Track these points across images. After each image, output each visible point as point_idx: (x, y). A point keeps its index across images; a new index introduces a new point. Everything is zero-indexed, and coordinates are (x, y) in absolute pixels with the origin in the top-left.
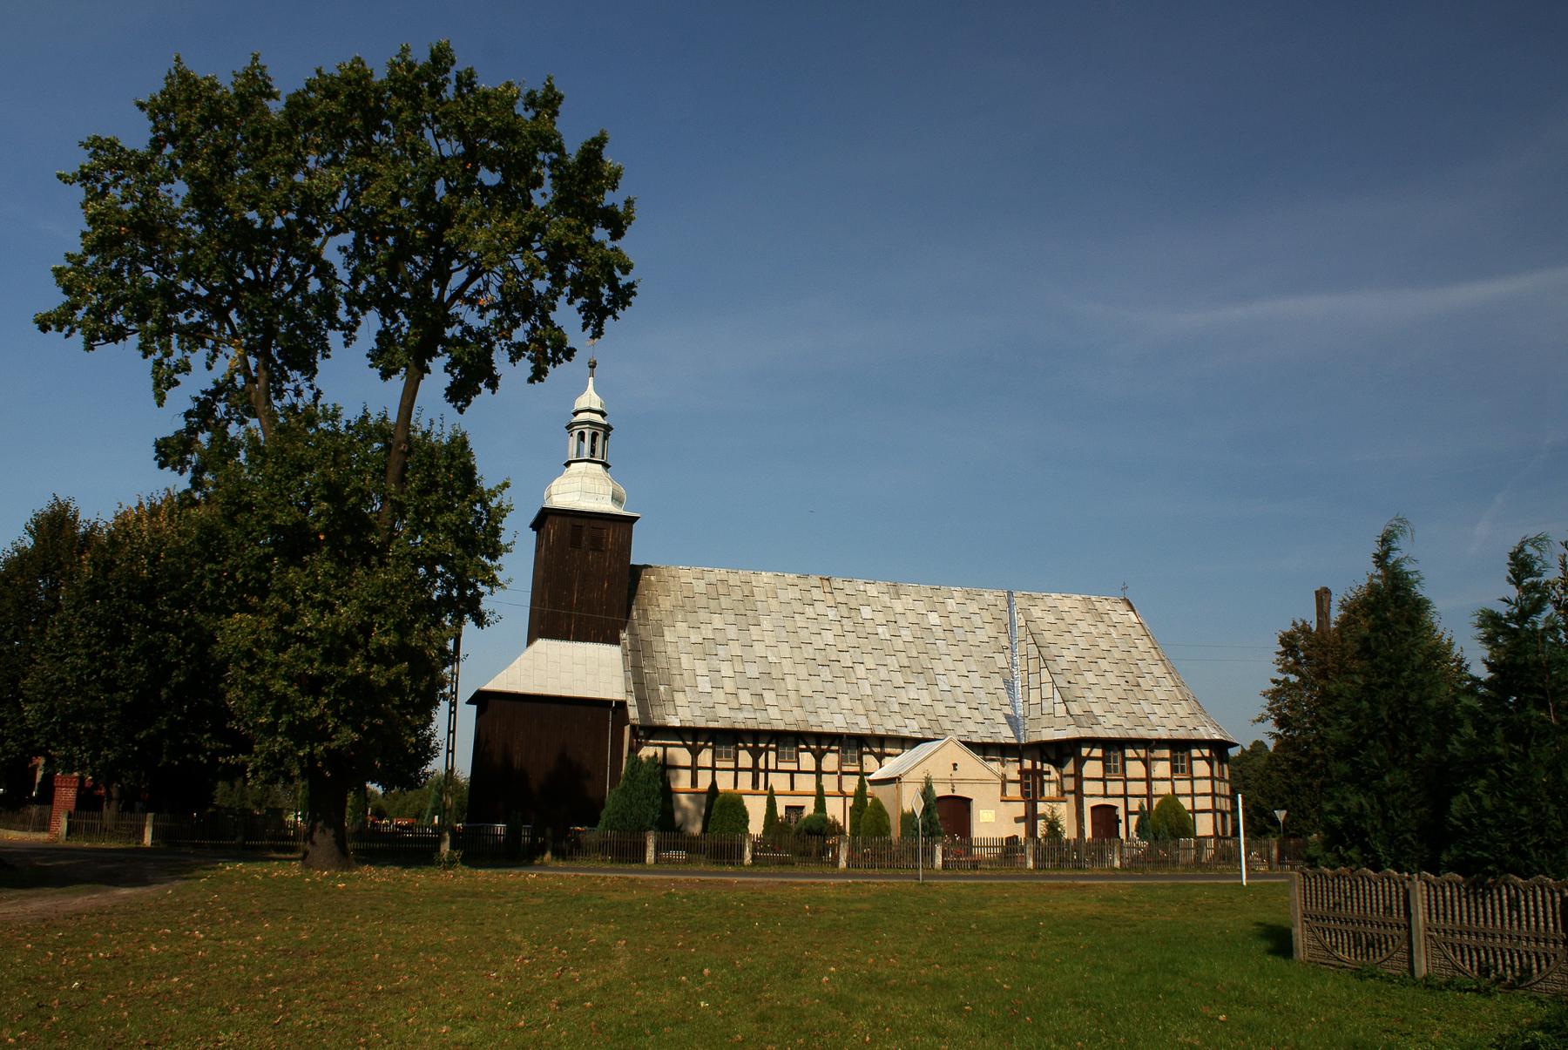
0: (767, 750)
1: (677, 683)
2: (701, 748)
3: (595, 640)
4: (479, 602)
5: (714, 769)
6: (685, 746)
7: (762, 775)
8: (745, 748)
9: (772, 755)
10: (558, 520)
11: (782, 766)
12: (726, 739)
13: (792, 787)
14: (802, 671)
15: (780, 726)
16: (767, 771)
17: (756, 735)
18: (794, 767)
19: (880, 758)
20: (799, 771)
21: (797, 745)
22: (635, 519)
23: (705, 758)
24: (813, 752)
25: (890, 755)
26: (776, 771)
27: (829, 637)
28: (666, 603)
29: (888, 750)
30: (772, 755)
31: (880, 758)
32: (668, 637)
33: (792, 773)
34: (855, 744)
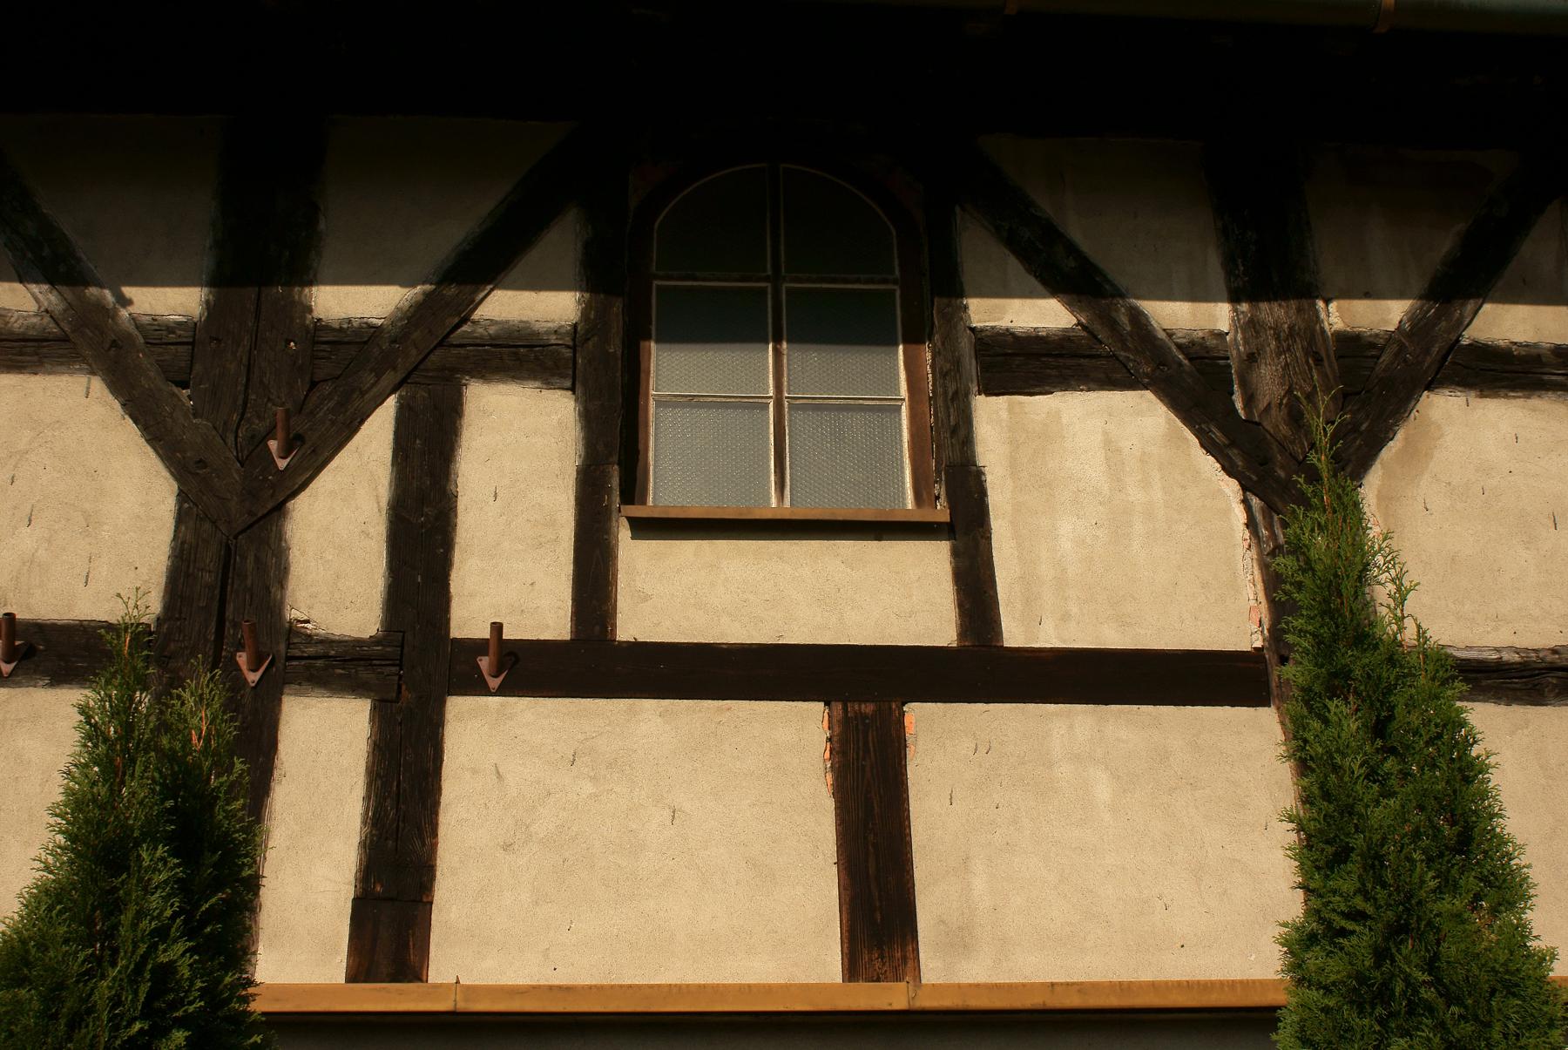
0: (430, 374)
7: (324, 747)
9: (519, 443)
11: (672, 593)
16: (416, 669)
18: (895, 597)
20: (981, 666)
24: (1196, 388)
26: (591, 661)
30: (519, 443)
33: (864, 691)
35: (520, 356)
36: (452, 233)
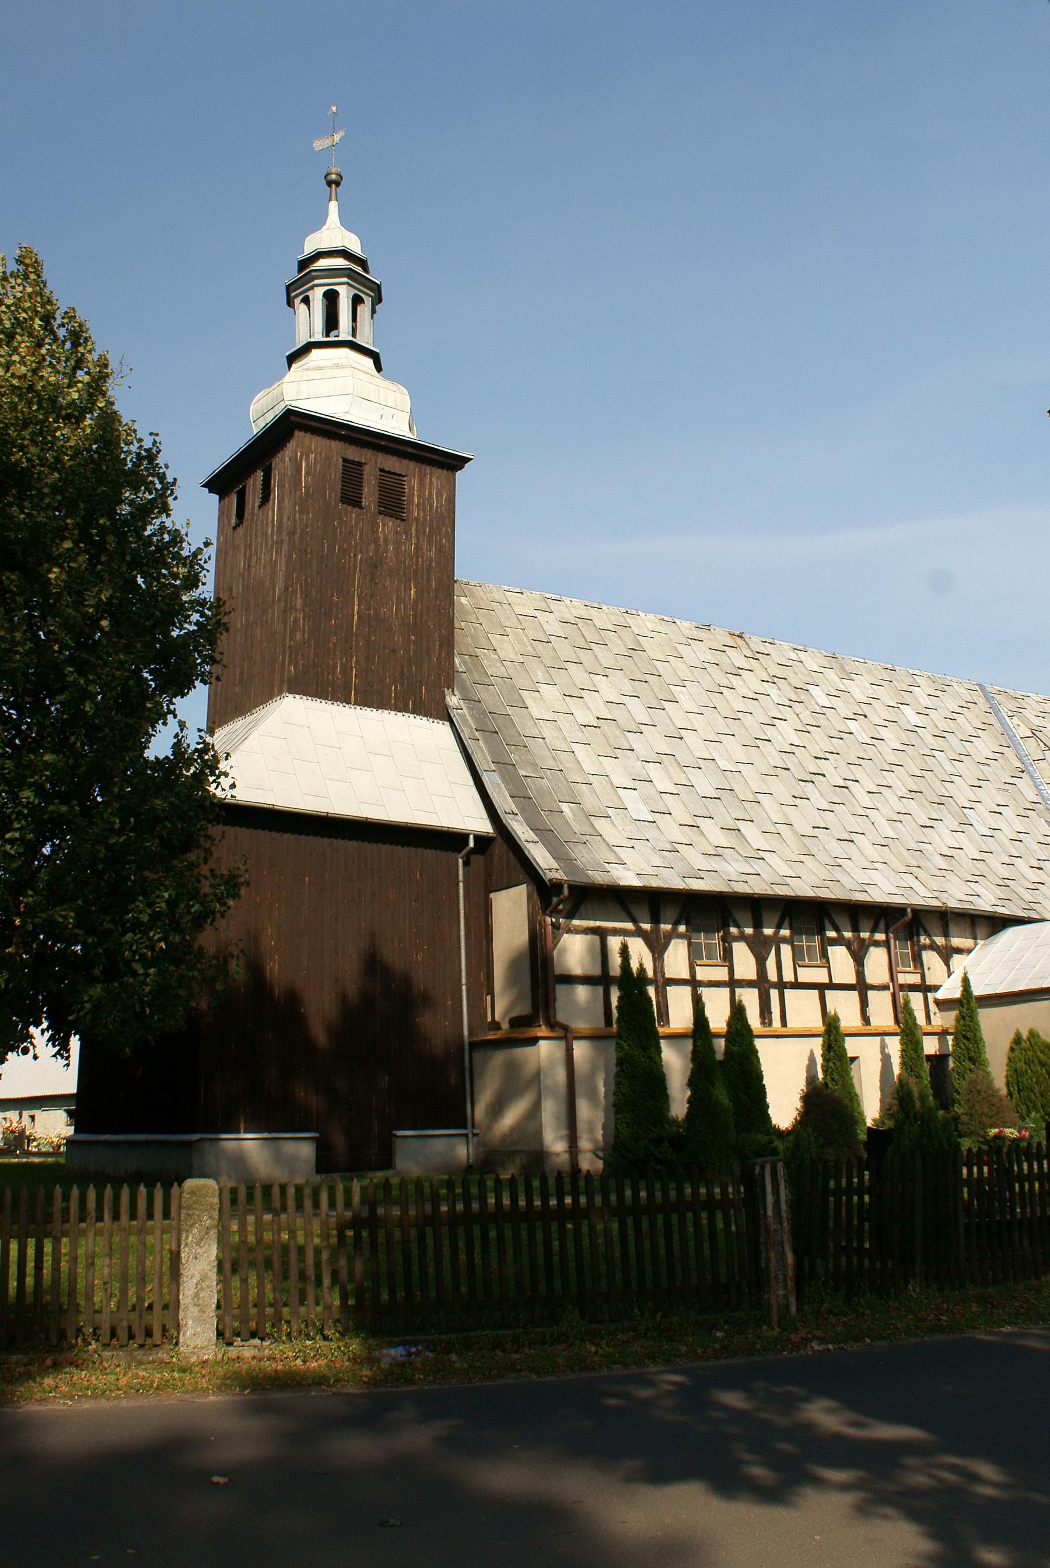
1: (589, 802)
2: (669, 937)
3: (401, 707)
4: (12, 1051)
5: (693, 983)
6: (639, 933)
7: (774, 994)
8: (742, 937)
9: (786, 950)
10: (317, 444)
11: (806, 975)
12: (709, 913)
13: (866, 1020)
14: (781, 788)
15: (803, 889)
17: (757, 907)
18: (819, 976)
19: (947, 954)
20: (832, 986)
21: (821, 932)
22: (468, 460)
23: (677, 958)
24: (848, 944)
25: (959, 951)
26: (797, 985)
27: (786, 733)
28: (507, 649)
29: (956, 942)
30: (786, 950)
31: (947, 954)
32: (535, 710)
34: (909, 925)
35: (785, 940)
36: (775, 920)
